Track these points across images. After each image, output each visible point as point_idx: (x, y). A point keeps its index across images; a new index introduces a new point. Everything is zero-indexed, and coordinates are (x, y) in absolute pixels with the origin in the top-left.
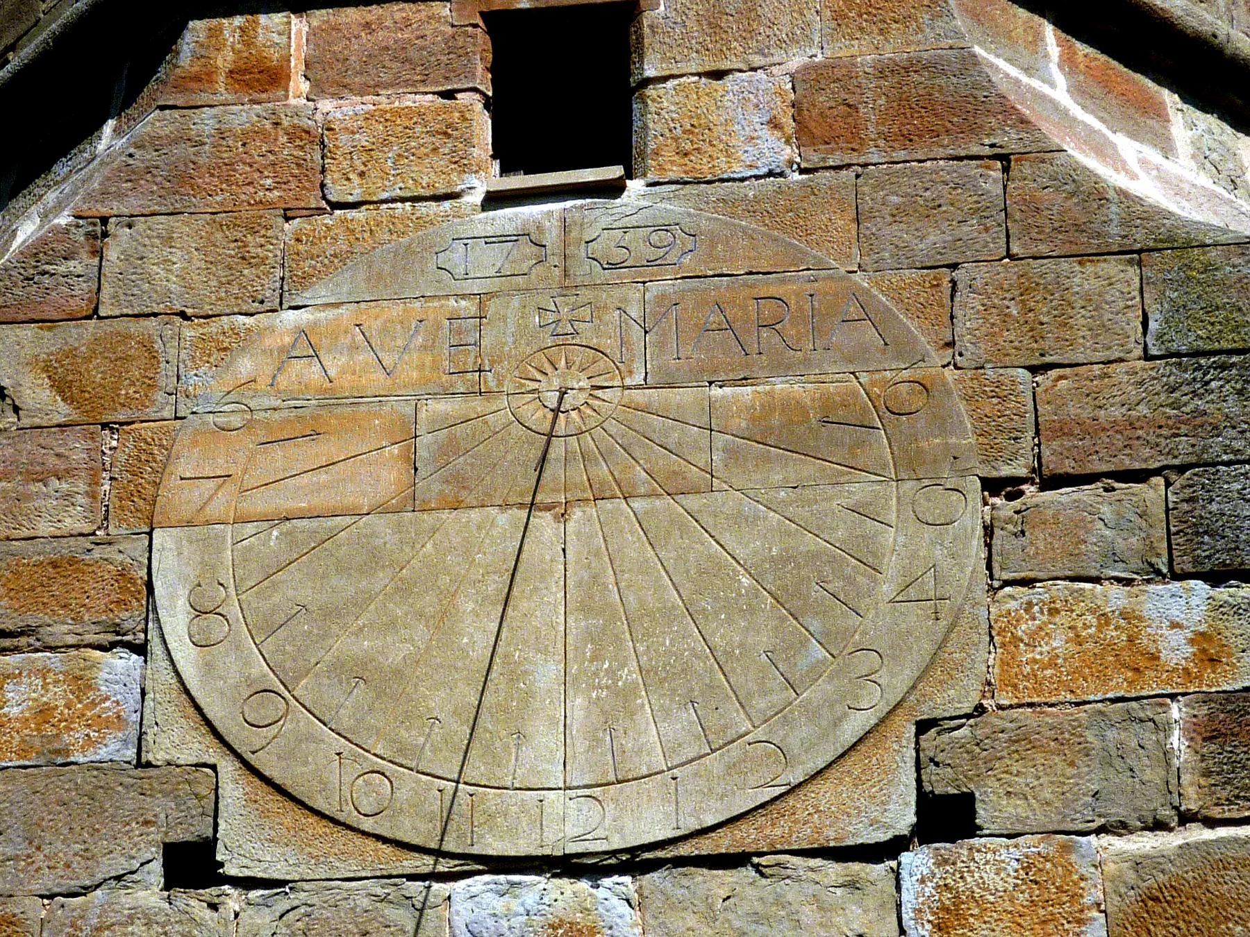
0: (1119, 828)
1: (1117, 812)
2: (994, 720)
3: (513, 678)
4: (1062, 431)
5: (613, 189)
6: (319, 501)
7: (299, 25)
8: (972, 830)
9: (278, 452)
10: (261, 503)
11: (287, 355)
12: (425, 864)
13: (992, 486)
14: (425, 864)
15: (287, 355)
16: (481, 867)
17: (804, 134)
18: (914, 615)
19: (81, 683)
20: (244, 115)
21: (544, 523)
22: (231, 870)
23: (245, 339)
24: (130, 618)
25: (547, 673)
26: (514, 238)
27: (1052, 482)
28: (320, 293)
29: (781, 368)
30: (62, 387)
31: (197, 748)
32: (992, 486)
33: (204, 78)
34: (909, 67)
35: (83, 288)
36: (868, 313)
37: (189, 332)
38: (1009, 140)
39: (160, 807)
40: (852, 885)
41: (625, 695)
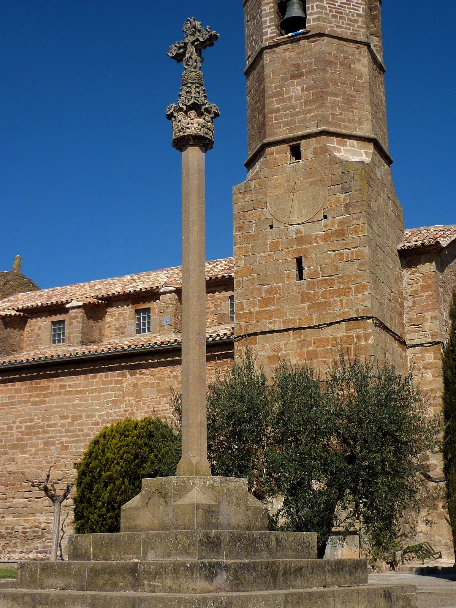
0: (338, 216)
1: (338, 215)
2: (329, 208)
3: (293, 208)
4: (334, 181)
5: (299, 161)
6: (279, 194)
7: (274, 148)
8: (327, 218)
9: (275, 190)
10: (275, 194)
11: (275, 180)
12: (287, 225)
13: (328, 186)
14: (287, 225)
15: (275, 180)
16: (449, 519)
17: (314, 154)
18: (323, 199)
19: (262, 212)
20: (271, 157)
21: (295, 193)
22: (80, 310)
23: (272, 179)
24: (265, 206)
25: (296, 208)
26: (291, 167)
27: (333, 186)
28: (277, 174)
29: (312, 177)
30: (259, 185)
31: (271, 217)
32: (328, 186)
33: (268, 154)
34: (321, 147)
35: (260, 176)
36: (319, 171)
37: (268, 179)
38: (329, 153)
39: (269, 222)
40: (319, 223)
41: (302, 209)
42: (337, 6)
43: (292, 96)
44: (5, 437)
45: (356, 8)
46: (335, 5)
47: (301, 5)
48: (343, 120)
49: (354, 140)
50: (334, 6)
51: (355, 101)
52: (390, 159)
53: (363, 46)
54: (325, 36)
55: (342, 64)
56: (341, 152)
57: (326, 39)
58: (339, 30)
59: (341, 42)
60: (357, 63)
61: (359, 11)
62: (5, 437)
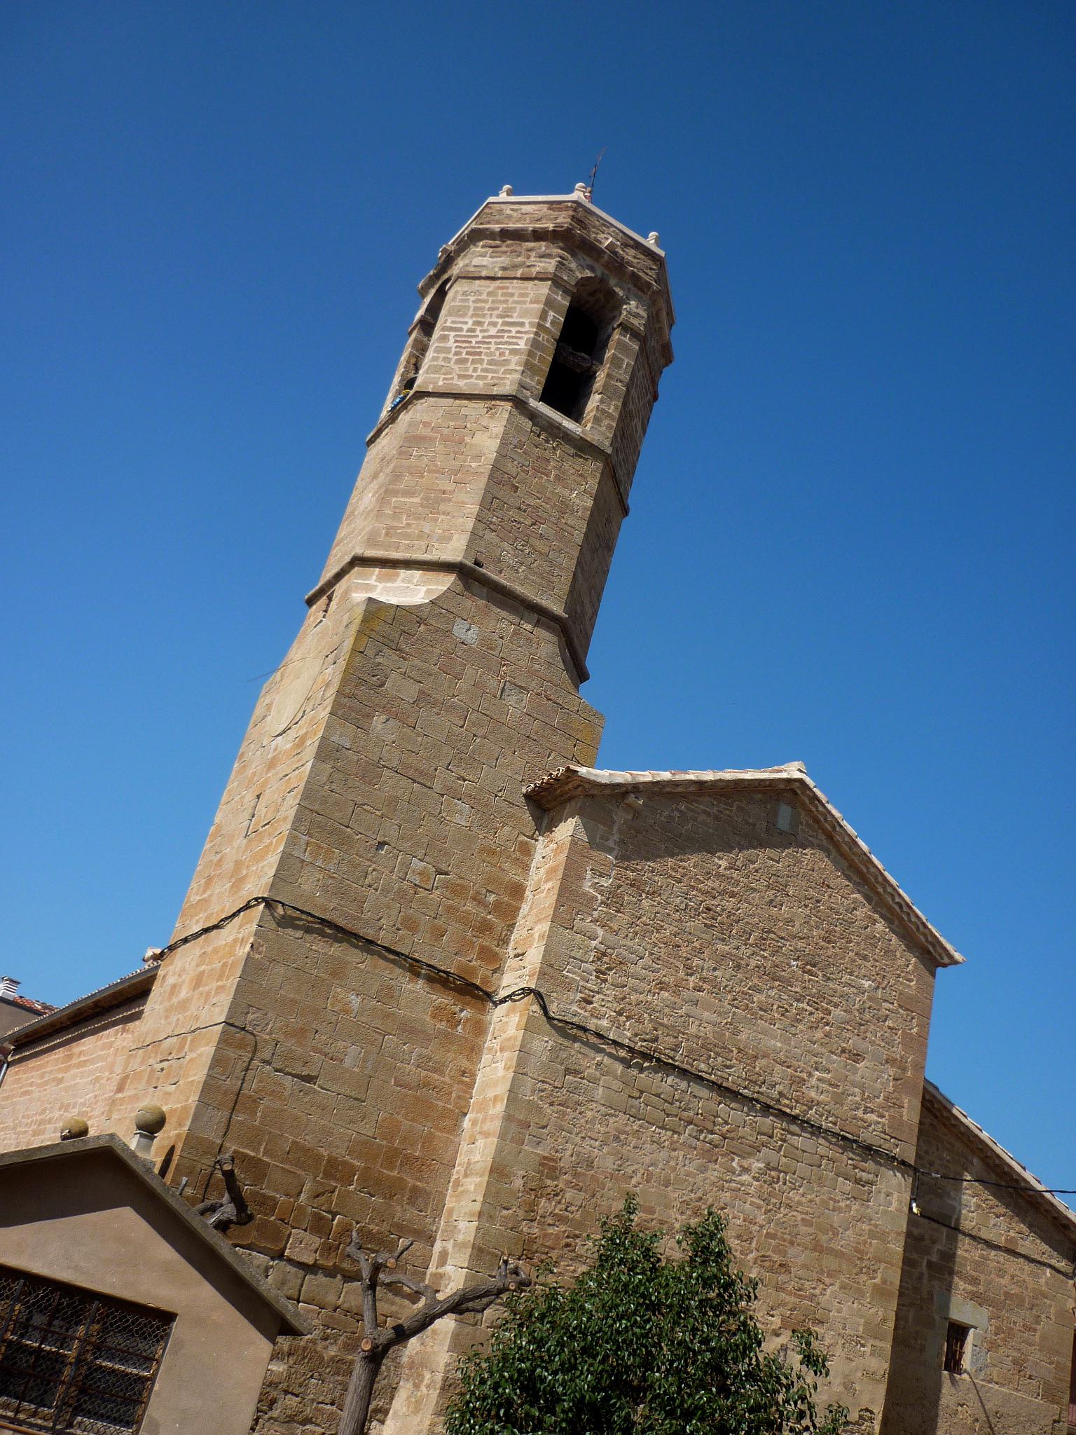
42: (473, 344)
43: (471, 317)
44: (467, 347)
45: (514, 340)
46: (471, 342)
47: (473, 1001)
48: (407, 536)
49: (418, 569)
50: (468, 345)
51: (449, 500)
52: (393, 378)
53: (502, 403)
54: (427, 396)
55: (445, 440)
56: (376, 586)
57: (432, 400)
58: (462, 383)
59: (458, 402)
60: (478, 435)
61: (518, 345)
62: (467, 347)
